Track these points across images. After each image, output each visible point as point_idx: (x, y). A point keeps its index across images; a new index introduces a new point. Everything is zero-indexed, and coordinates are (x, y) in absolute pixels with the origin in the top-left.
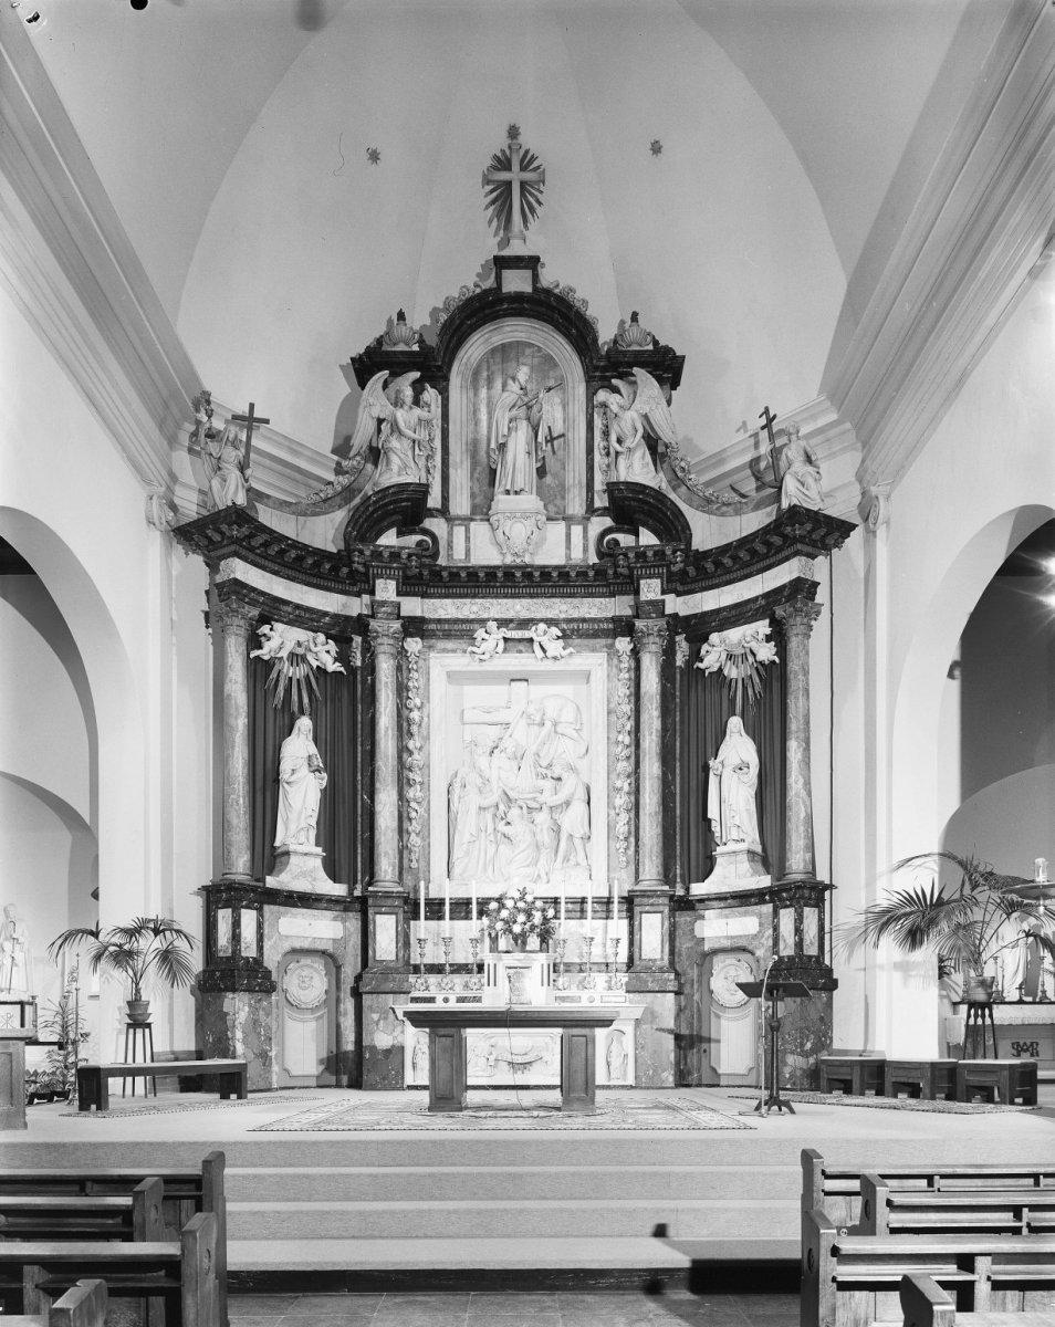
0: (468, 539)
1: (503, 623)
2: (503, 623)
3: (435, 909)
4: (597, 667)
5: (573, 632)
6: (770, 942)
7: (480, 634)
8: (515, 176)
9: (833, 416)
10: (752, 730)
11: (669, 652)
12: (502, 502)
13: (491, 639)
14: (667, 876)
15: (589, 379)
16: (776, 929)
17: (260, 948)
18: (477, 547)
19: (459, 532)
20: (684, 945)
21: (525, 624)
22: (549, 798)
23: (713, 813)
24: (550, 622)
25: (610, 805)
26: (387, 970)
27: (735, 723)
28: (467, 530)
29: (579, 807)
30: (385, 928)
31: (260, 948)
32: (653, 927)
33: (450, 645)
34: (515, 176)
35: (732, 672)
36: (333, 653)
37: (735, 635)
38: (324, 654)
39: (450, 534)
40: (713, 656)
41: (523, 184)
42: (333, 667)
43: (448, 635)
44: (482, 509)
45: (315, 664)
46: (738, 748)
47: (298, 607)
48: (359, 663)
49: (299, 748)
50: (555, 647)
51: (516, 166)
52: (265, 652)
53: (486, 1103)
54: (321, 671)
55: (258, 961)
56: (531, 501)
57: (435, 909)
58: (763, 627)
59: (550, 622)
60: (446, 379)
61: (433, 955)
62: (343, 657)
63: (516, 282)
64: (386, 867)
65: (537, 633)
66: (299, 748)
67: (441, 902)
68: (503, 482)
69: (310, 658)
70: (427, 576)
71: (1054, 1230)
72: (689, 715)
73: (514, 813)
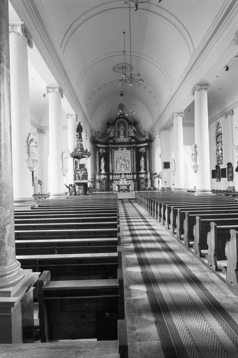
1: (121, 147)
3: (115, 174)
4: (129, 152)
5: (128, 148)
7: (119, 148)
8: (121, 107)
9: (133, 287)
12: (120, 136)
13: (120, 149)
14: (137, 171)
15: (128, 124)
18: (119, 140)
19: (117, 139)
22: (125, 164)
23: (141, 165)
24: (125, 147)
26: (111, 180)
27: (142, 157)
29: (128, 165)
30: (111, 177)
32: (135, 176)
34: (121, 107)
35: (142, 152)
37: (143, 149)
38: (104, 151)
40: (140, 150)
41: (122, 107)
42: (105, 152)
44: (119, 137)
46: (143, 159)
49: (102, 160)
50: (126, 150)
52: (100, 152)
53: (10, 146)
56: (123, 136)
57: (115, 174)
58: (144, 148)
61: (115, 179)
62: (106, 151)
63: (121, 116)
64: (111, 171)
65: (124, 149)
66: (102, 160)
67: (116, 174)
68: (120, 135)
70: (114, 143)
71: (237, 206)
72: (138, 156)
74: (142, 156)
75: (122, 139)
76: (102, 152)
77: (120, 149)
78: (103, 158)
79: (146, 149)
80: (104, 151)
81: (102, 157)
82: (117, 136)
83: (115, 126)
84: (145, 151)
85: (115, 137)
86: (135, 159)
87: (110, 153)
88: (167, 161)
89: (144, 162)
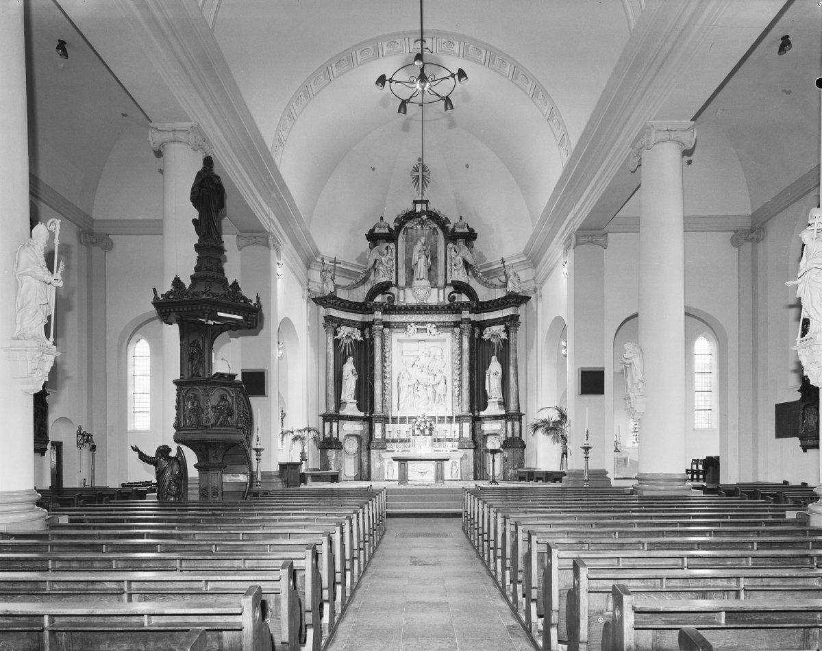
0: (404, 294)
1: (416, 323)
2: (416, 323)
6: (505, 432)
7: (409, 327)
10: (500, 361)
11: (472, 333)
13: (412, 328)
16: (506, 428)
17: (338, 434)
20: (478, 432)
21: (424, 323)
23: (487, 388)
24: (432, 323)
25: (453, 384)
27: (494, 358)
28: (404, 291)
31: (338, 434)
33: (398, 330)
36: (360, 334)
38: (357, 336)
39: (399, 293)
41: (423, 176)
43: (398, 327)
44: (409, 284)
45: (354, 338)
46: (495, 367)
47: (349, 320)
48: (368, 337)
50: (434, 331)
51: (420, 170)
52: (338, 337)
54: (356, 340)
55: (338, 439)
59: (432, 323)
60: (397, 240)
62: (363, 335)
66: (349, 367)
69: (352, 337)
73: (420, 387)
74: (493, 355)
75: (422, 292)
76: (348, 337)
77: (412, 328)
78: (351, 359)
79: (507, 330)
80: (357, 336)
81: (349, 355)
82: (402, 282)
83: (396, 245)
84: (503, 336)
85: (396, 285)
86: (466, 365)
87: (378, 341)
88: (591, 365)
89: (500, 375)
